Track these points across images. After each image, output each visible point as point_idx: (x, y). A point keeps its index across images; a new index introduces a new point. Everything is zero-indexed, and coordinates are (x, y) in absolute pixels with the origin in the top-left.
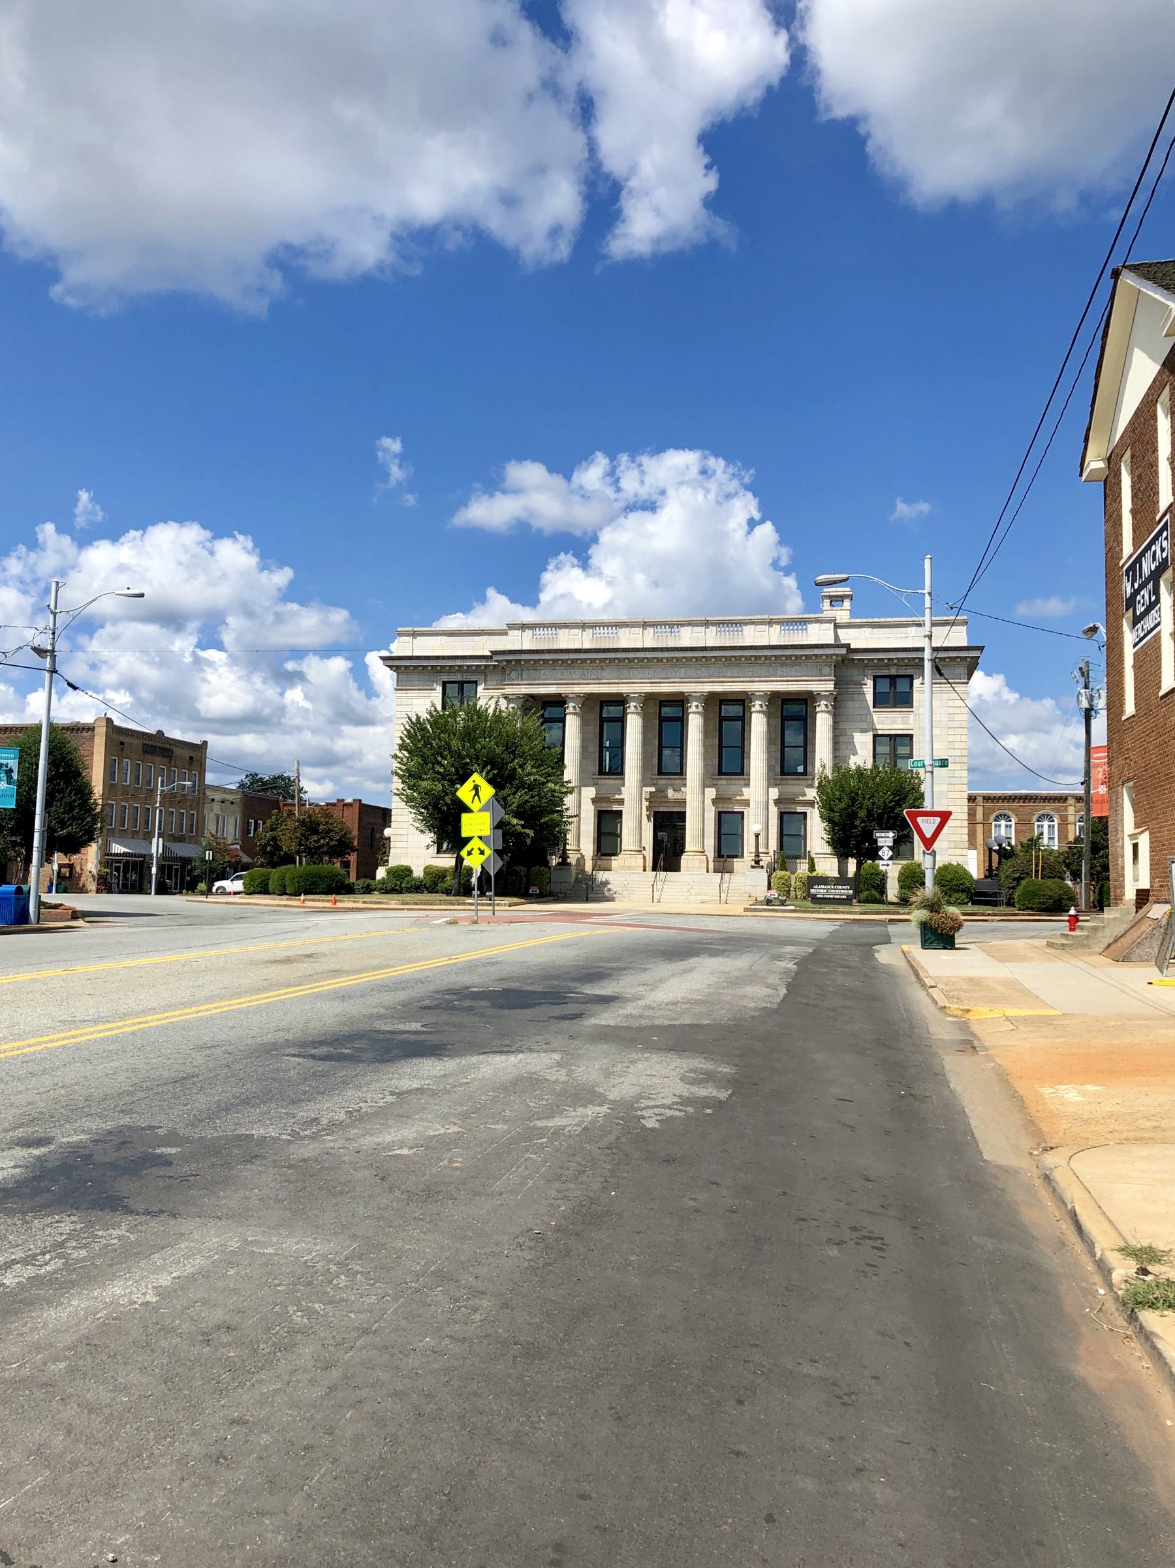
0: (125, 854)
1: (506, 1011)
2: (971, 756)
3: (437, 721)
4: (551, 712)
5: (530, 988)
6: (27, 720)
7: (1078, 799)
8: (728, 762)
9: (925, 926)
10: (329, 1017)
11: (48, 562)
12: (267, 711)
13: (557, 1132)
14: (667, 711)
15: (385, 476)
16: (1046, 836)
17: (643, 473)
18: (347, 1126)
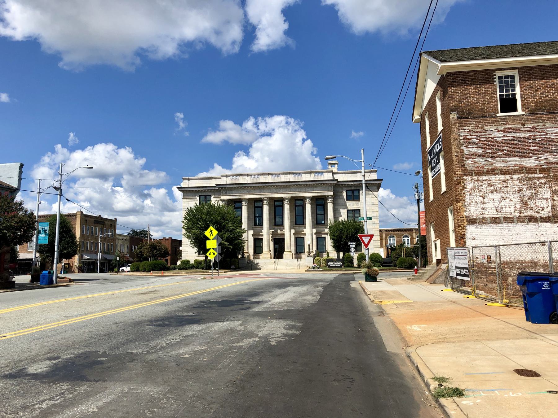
0: (88, 259)
1: (223, 308)
2: (380, 216)
3: (197, 208)
4: (237, 205)
5: (231, 300)
6: (52, 213)
7: (416, 230)
8: (298, 221)
9: (366, 274)
10: (161, 311)
11: (59, 158)
12: (138, 208)
13: (241, 347)
14: (277, 204)
15: (178, 126)
16: (406, 243)
17: (266, 123)
18: (167, 348)
